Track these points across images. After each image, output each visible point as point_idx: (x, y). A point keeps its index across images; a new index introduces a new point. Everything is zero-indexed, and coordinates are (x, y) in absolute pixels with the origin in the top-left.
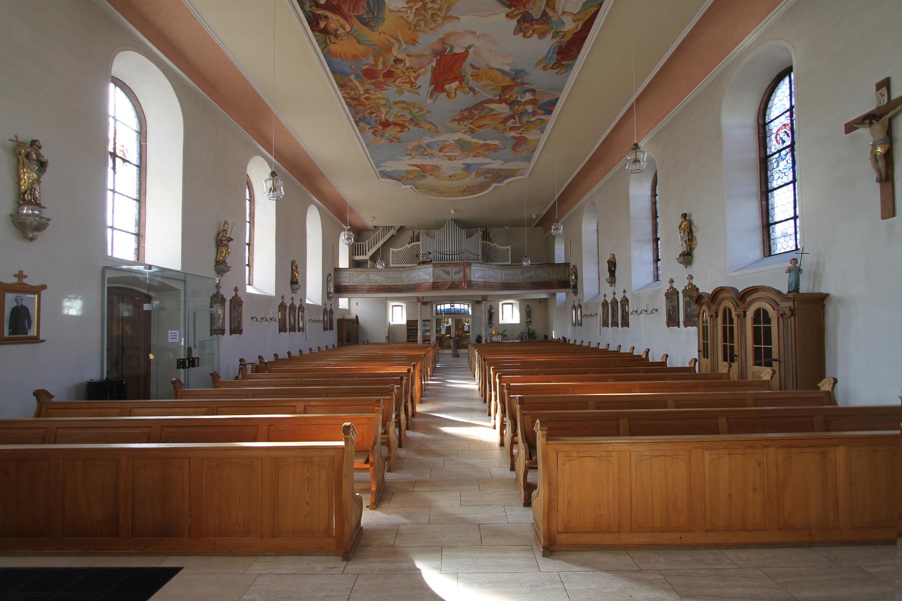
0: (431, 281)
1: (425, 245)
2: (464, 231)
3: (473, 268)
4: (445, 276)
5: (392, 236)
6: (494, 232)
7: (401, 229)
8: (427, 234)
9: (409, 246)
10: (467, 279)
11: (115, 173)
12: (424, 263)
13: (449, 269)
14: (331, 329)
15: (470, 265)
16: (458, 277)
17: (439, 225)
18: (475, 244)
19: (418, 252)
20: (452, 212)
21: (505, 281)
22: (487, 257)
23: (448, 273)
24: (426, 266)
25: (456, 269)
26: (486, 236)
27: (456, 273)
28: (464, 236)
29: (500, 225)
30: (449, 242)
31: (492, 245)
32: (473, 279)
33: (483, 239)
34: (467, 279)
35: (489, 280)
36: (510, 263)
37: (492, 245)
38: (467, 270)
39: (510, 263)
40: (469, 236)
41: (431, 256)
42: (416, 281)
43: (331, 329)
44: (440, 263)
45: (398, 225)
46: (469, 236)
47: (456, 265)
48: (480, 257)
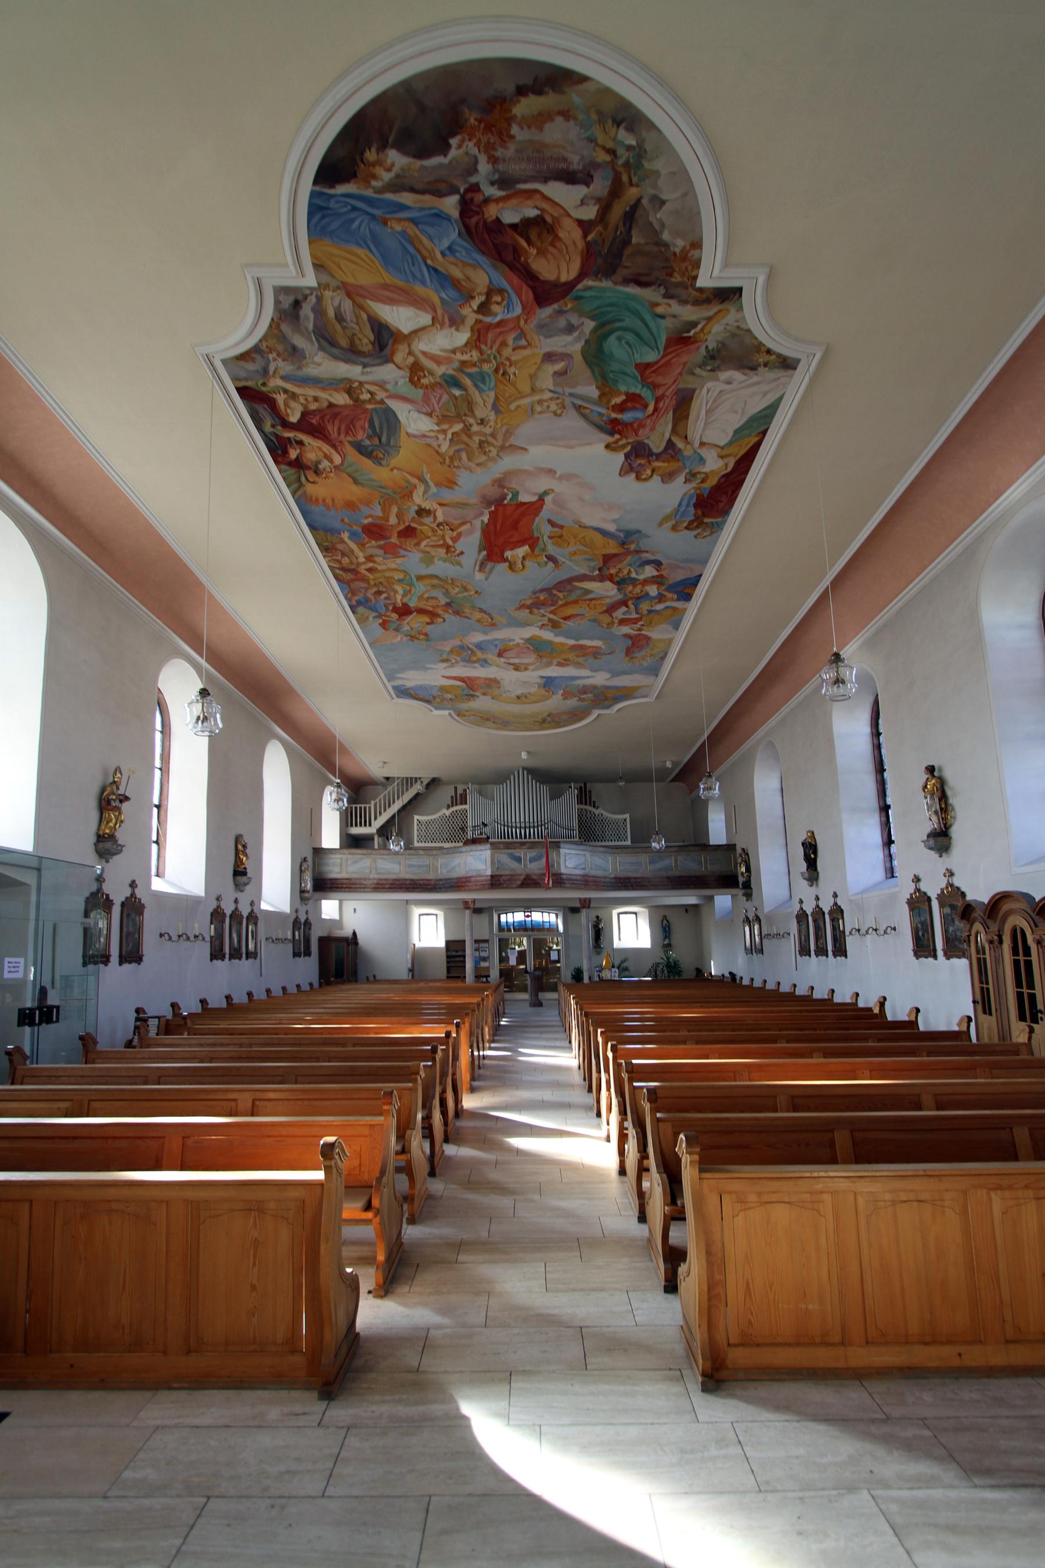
0: (489, 873)
1: (474, 812)
2: (545, 789)
3: (562, 851)
4: (514, 865)
5: (418, 795)
6: (598, 790)
7: (434, 783)
8: (480, 793)
9: (447, 813)
12: (474, 841)
13: (520, 853)
15: (557, 845)
16: (536, 867)
17: (501, 778)
18: (566, 809)
19: (465, 821)
20: (524, 755)
22: (588, 833)
23: (518, 860)
24: (478, 847)
25: (531, 853)
26: (584, 797)
29: (610, 778)
30: (521, 806)
31: (597, 812)
33: (580, 802)
35: (593, 873)
36: (629, 843)
37: (597, 812)
38: (553, 855)
39: (629, 843)
40: (554, 796)
41: (487, 830)
42: (460, 872)
45: (427, 776)
46: (554, 796)
47: (533, 845)
48: (576, 833)
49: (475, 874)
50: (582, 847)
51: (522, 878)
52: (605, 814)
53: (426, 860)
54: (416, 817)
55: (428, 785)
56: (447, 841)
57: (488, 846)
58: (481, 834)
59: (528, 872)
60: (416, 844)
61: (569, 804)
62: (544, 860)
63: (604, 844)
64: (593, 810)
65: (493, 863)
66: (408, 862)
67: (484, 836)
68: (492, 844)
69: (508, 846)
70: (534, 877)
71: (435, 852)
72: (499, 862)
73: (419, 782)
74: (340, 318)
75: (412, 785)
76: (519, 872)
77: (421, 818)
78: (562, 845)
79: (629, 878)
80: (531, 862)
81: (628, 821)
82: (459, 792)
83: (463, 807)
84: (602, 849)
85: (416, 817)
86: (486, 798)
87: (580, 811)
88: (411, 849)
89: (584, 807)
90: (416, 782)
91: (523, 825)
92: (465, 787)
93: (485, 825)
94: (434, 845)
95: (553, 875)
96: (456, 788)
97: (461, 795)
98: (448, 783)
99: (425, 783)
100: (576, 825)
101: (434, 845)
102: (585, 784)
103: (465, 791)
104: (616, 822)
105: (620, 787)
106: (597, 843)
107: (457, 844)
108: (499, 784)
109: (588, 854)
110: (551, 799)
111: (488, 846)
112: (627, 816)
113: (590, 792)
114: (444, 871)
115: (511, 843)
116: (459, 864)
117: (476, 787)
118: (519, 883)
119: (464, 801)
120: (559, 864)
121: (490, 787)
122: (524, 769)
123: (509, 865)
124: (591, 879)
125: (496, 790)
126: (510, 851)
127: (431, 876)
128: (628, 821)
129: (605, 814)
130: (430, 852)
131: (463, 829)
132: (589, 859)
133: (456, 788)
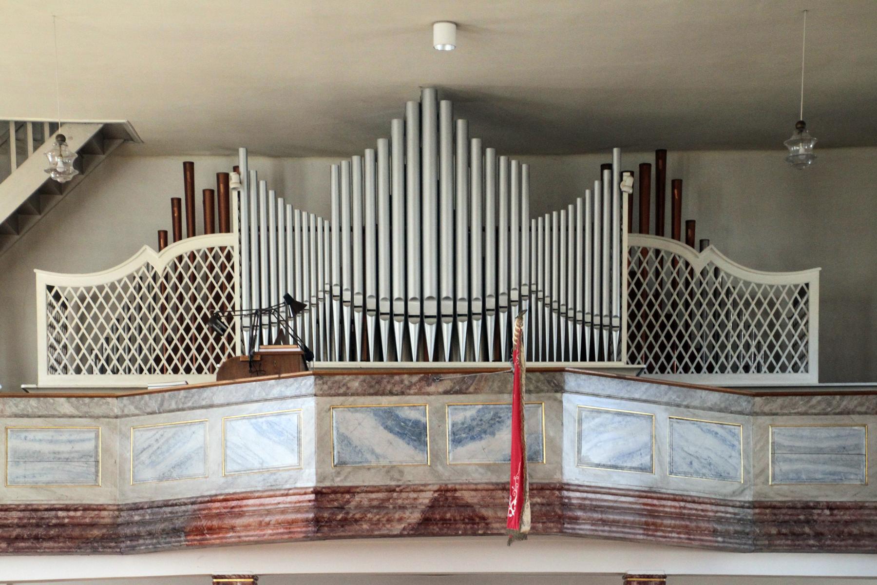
0: (308, 480)
1: (267, 255)
2: (515, 172)
3: (571, 402)
4: (401, 453)
5: (47, 192)
6: (711, 178)
7: (108, 145)
8: (279, 188)
9: (161, 261)
10: (537, 473)
11: (429, 485)
12: (257, 366)
13: (415, 407)
14: (687, 222)
15: (553, 383)
16: (476, 461)
17: (355, 129)
18: (590, 251)
19: (222, 295)
20: (442, 38)
21: (780, 492)
22: (665, 337)
23: (414, 433)
24: (272, 386)
25: (462, 411)
26: (657, 204)
27: (464, 434)
28: (518, 202)
29: (756, 132)
30: (422, 236)
31: (699, 261)
32: (571, 473)
33: (639, 225)
34: (537, 473)
35: (677, 484)
36: (810, 378)
37: (699, 261)
38: (537, 417)
39: (810, 378)
40: (547, 201)
41: (304, 325)
42: (202, 480)
43: (687, 222)
44: (362, 356)
45: (82, 118)
46: (547, 201)
47: (466, 383)
48: (620, 338)
49: (256, 483)
50: (641, 390)
51: (426, 498)
52: (731, 269)
53: (79, 436)
54: (43, 278)
55: (86, 154)
56: (159, 365)
57: (308, 383)
58: (282, 338)
59: (448, 477)
60: (45, 380)
61: (601, 222)
62: (505, 436)
63: (718, 379)
64: (678, 248)
65: (322, 441)
66: (14, 443)
67: (292, 348)
68: (319, 375)
69: (377, 383)
70: (468, 497)
71: (115, 406)
72: (344, 439)
73: (51, 142)
74: (20, 518)
75: (23, 154)
76: (412, 477)
77: (63, 281)
78: (571, 381)
79: (807, 507)
80: (457, 441)
81: (814, 295)
82: (204, 181)
83: (217, 240)
84: (714, 398)
85: (43, 278)
86: (300, 205)
87: (639, 255)
88: (26, 394)
89: (651, 241)
90: (39, 141)
91: (431, 308)
92: (222, 164)
93: (297, 308)
94: (109, 381)
95: (541, 489)
96: (189, 168)
97: (209, 194)
98: (161, 150)
99: (74, 145)
100: (619, 308)
101: (109, 381)
102: (661, 155)
103: (223, 179)
104: (767, 302)
105: (796, 163)
106: (692, 378)
107: (194, 379)
108: (347, 155)
109: (661, 414)
110: (533, 215)
111: (308, 383)
112: (811, 277)
113: (677, 184)
114: (148, 474)
115: (391, 373)
116: (203, 452)
117: (264, 164)
118: (415, 517)
119: (219, 221)
120: (557, 450)
121: (314, 165)
122: (440, 94)
123: (379, 451)
124: (669, 506)
125: (331, 176)
126: (386, 401)
127: (102, 495)
128: (814, 295)
129: (731, 269)
130: (98, 407)
131: (217, 321)
132: (664, 430)
133: (189, 168)
